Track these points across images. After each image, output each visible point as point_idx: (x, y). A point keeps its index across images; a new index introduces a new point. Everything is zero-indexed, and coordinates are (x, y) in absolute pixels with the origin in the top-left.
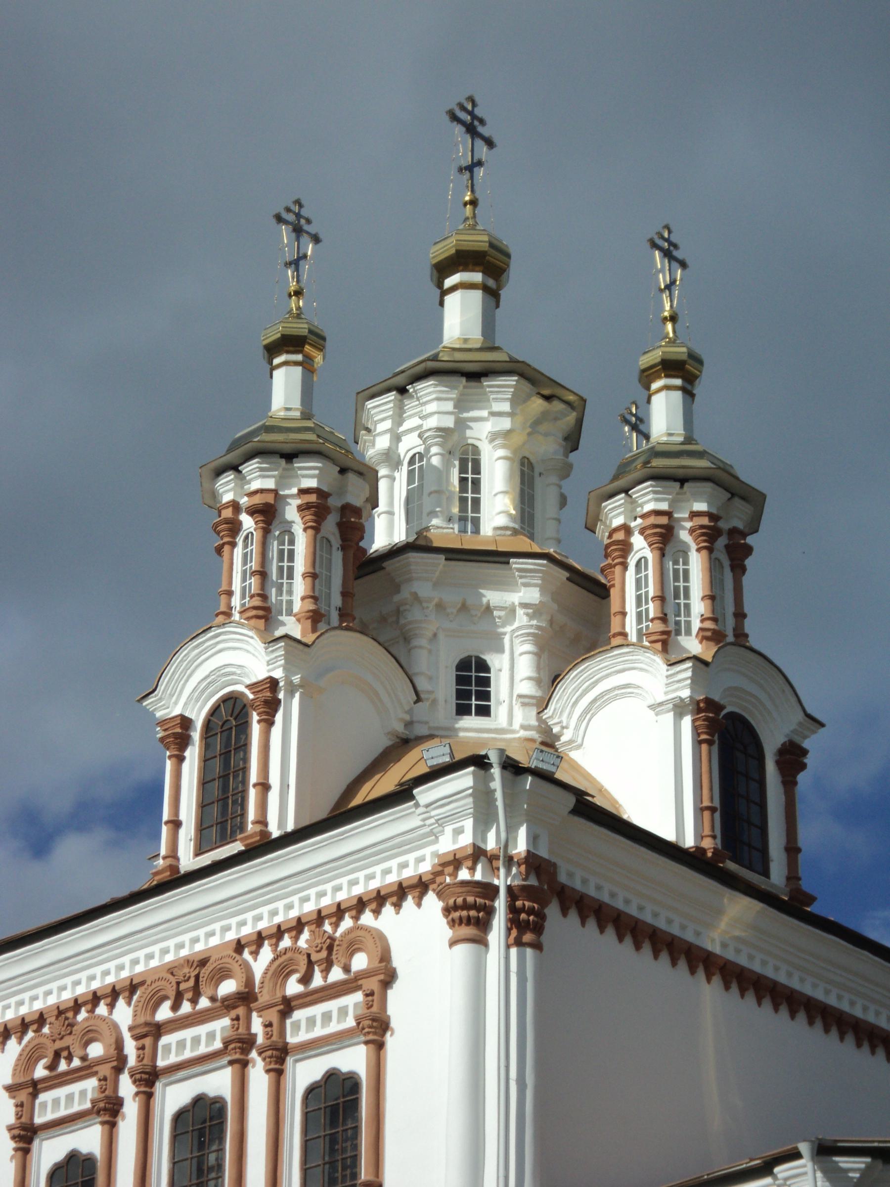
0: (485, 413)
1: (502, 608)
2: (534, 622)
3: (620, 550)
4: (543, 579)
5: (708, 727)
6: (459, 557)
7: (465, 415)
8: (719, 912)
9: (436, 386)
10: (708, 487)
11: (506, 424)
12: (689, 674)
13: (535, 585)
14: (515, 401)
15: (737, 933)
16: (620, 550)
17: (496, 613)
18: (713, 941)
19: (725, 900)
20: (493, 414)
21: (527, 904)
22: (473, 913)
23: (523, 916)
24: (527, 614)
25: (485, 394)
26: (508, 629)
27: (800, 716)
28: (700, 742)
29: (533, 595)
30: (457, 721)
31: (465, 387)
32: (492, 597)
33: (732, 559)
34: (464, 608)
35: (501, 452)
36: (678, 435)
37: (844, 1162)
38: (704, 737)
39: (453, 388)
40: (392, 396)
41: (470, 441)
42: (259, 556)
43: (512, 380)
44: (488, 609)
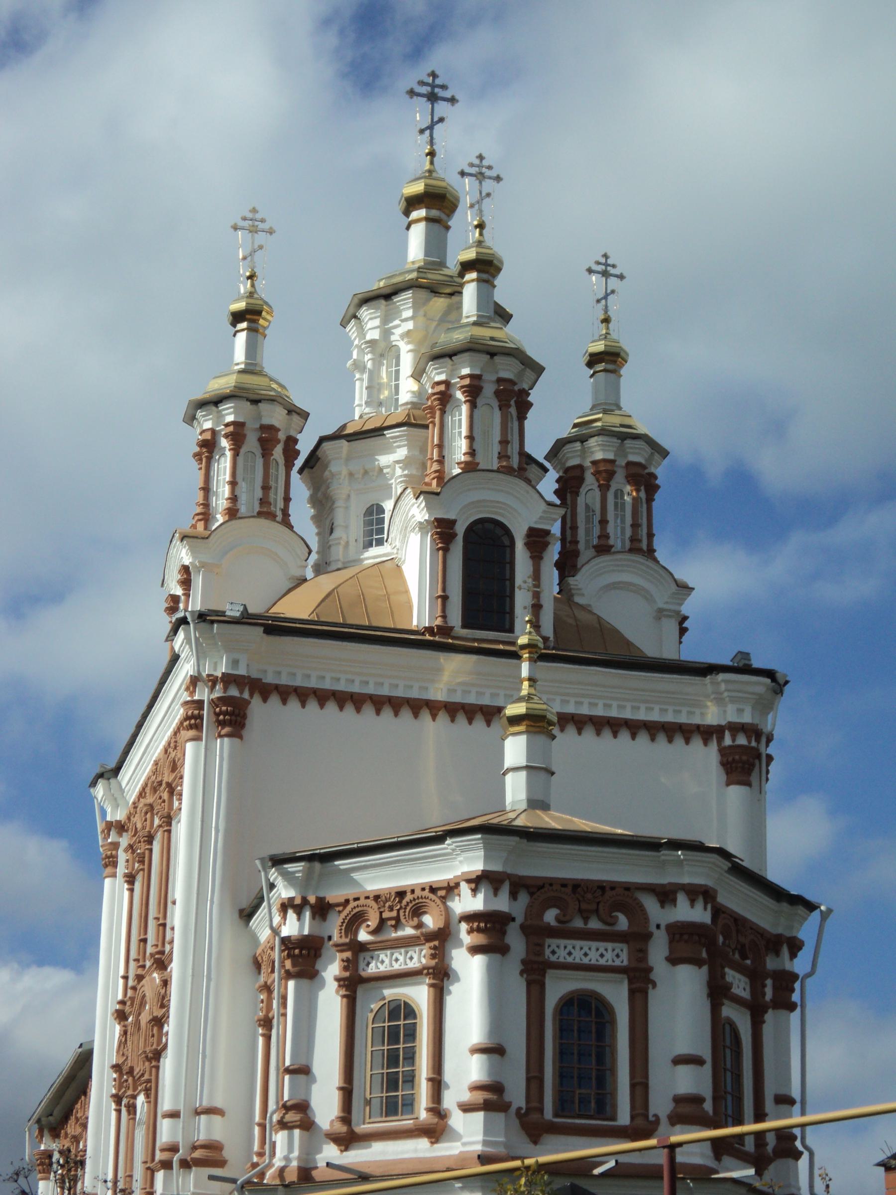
0: (397, 322)
1: (388, 467)
2: (406, 472)
3: (430, 413)
4: (407, 440)
5: (440, 538)
6: (361, 437)
7: (391, 325)
8: (439, 670)
9: (367, 310)
10: (466, 356)
11: (410, 325)
12: (424, 504)
13: (404, 446)
14: (416, 307)
15: (460, 680)
16: (430, 413)
17: (385, 471)
18: (438, 693)
19: (442, 660)
20: (402, 321)
21: (224, 708)
22: (193, 721)
23: (221, 717)
24: (400, 468)
25: (398, 307)
26: (393, 481)
27: (543, 506)
28: (438, 549)
29: (402, 453)
30: (362, 553)
31: (386, 306)
32: (384, 460)
33: (263, 449)
34: (366, 472)
35: (410, 347)
36: (472, 316)
37: (291, 867)
38: (440, 545)
39: (377, 309)
40: (353, 322)
41: (394, 343)
42: (446, 424)
43: (408, 294)
44: (381, 470)
